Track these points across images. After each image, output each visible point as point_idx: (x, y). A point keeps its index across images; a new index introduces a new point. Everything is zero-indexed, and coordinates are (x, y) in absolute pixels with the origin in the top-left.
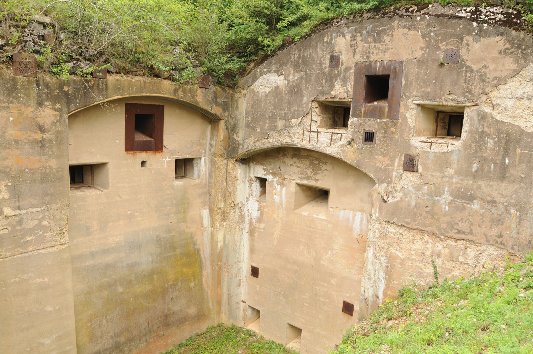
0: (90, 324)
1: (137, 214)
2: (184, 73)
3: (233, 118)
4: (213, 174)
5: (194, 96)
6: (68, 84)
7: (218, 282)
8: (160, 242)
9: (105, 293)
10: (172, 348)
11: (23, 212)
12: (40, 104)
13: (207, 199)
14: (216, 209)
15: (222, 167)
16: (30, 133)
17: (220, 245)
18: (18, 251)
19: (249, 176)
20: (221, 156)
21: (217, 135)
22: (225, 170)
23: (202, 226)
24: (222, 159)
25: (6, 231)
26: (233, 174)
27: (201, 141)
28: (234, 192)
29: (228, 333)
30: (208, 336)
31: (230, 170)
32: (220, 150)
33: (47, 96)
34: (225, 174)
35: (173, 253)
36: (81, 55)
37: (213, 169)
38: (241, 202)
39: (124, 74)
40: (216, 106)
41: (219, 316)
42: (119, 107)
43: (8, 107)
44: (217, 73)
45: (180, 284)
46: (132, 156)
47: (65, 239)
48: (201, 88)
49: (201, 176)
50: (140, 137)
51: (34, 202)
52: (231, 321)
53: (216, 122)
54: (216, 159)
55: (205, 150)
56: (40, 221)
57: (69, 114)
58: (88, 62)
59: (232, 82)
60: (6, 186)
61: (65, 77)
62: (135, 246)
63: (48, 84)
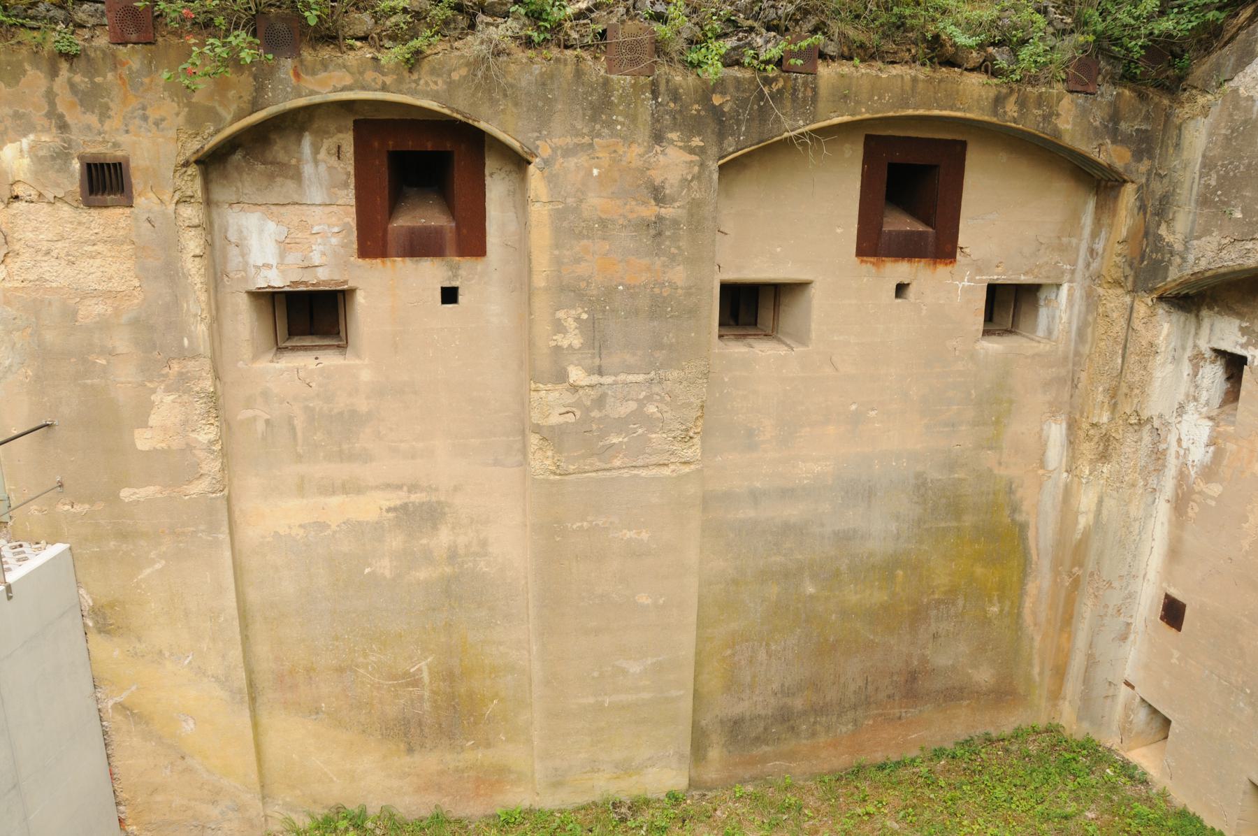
0: (729, 652)
1: (873, 413)
2: (1024, 53)
3: (1162, 177)
4: (1090, 330)
5: (1051, 114)
6: (720, 86)
7: (1067, 620)
8: (922, 490)
9: (773, 590)
10: (915, 752)
11: (608, 380)
12: (658, 137)
13: (1066, 397)
14: (1085, 426)
15: (1115, 315)
16: (634, 203)
17: (1083, 522)
18: (591, 464)
19: (1195, 346)
20: (1117, 283)
21: (1111, 226)
22: (1123, 322)
23: (1042, 464)
24: (1120, 291)
25: (570, 418)
26: (1144, 335)
27: (1065, 240)
28: (1144, 385)
29: (1068, 756)
30: (1014, 748)
31: (1137, 324)
32: (1116, 265)
33: (675, 118)
34: (1122, 335)
35: (954, 524)
36: (756, 18)
37: (1090, 319)
38: (1161, 416)
39: (862, 61)
40: (1113, 142)
41: (1055, 705)
42: (847, 146)
43: (591, 145)
44: (1127, 49)
45: (960, 603)
46: (873, 269)
47: (693, 451)
48: (1071, 92)
49: (1056, 333)
50: (899, 223)
51: (630, 359)
52: (1086, 726)
53: (1113, 188)
54: (1100, 290)
55: (1074, 264)
56: (641, 403)
57: (721, 162)
58: (773, 34)
59: (1170, 73)
60: (577, 319)
61: (714, 70)
62: (860, 491)
63: (676, 89)
